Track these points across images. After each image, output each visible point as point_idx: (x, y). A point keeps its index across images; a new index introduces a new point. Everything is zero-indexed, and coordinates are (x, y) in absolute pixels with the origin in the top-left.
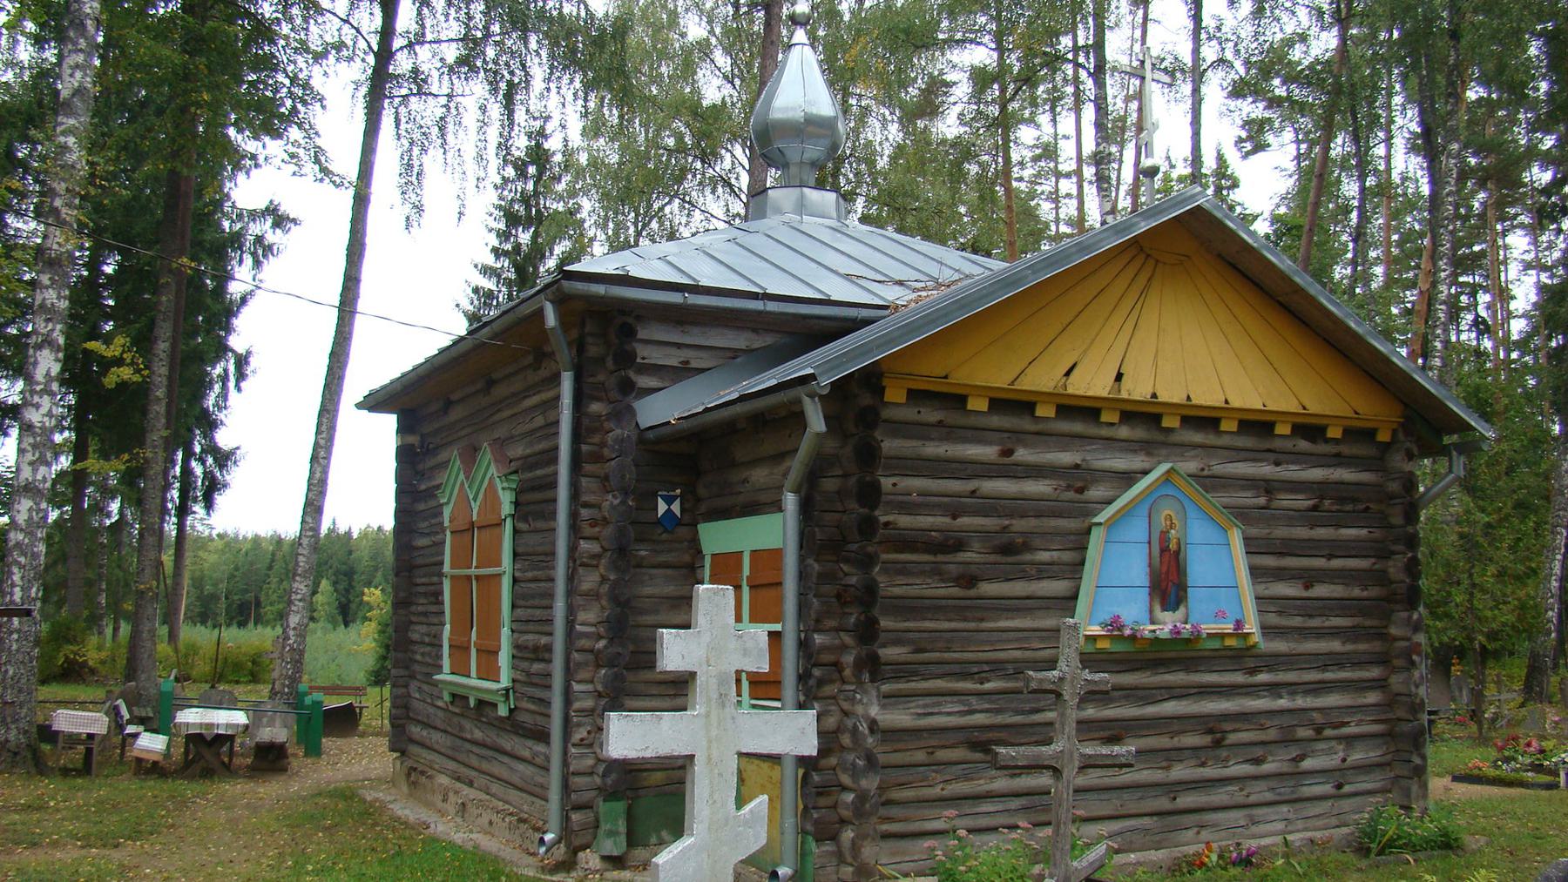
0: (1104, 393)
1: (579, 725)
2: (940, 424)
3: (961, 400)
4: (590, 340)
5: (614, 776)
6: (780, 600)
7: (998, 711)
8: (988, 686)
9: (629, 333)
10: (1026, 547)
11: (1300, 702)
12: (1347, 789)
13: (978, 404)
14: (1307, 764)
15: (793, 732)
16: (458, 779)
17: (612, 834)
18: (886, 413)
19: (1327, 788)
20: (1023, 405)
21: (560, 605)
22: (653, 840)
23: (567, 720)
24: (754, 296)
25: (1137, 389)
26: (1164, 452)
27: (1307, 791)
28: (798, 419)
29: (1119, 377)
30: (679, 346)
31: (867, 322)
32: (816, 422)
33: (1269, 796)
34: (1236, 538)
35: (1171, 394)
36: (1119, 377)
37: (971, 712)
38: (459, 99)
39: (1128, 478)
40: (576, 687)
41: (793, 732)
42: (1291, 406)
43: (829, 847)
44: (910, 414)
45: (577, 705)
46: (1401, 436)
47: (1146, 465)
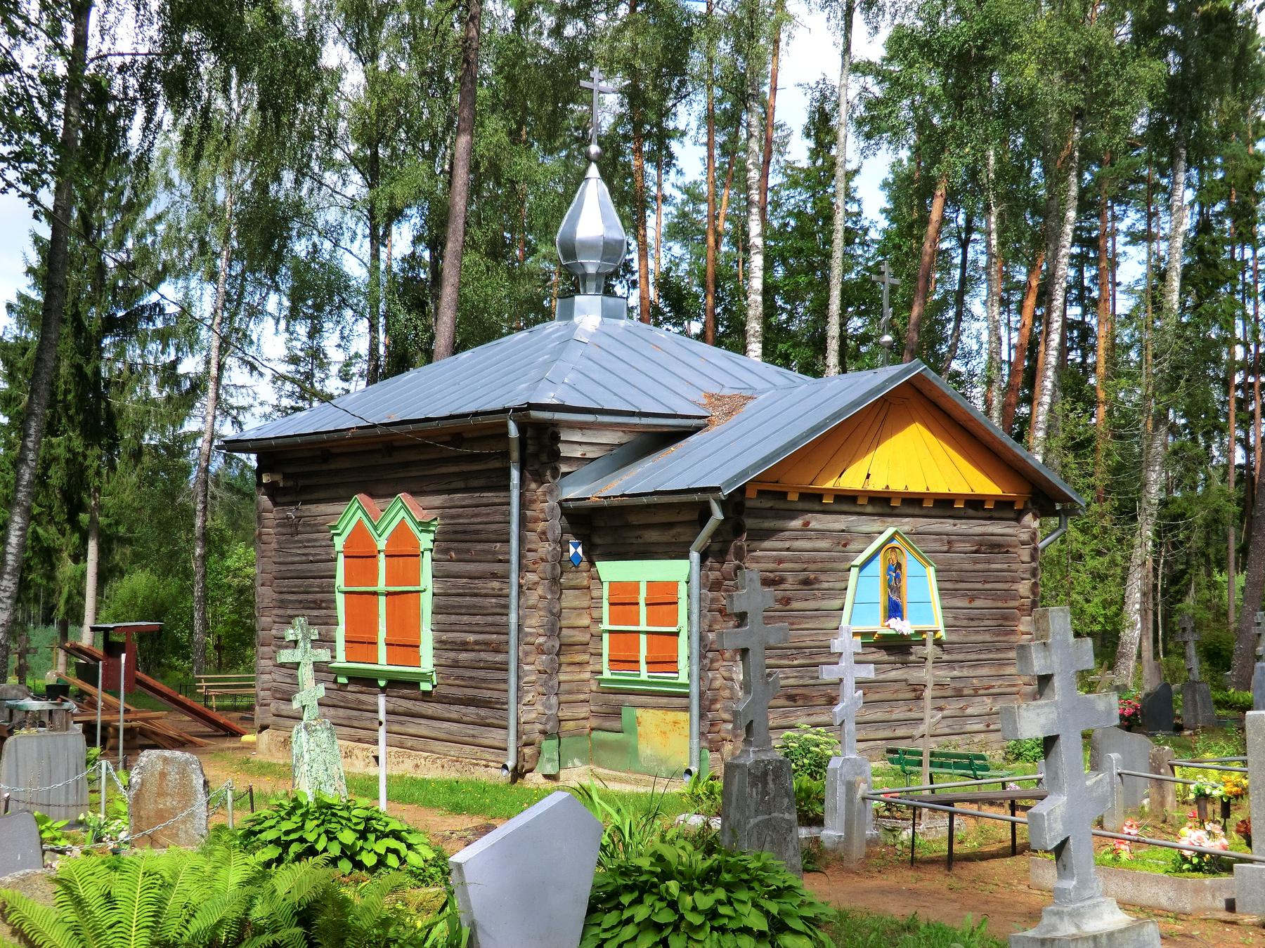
0: (859, 488)
1: (528, 692)
2: (771, 508)
3: (783, 495)
4: (529, 442)
5: (551, 723)
6: (675, 614)
7: (802, 677)
8: (796, 662)
9: (556, 438)
10: (817, 580)
11: (965, 673)
12: (992, 727)
13: (793, 497)
14: (969, 711)
15: (828, 674)
16: (359, 740)
17: (550, 760)
18: (748, 504)
19: (981, 727)
20: (817, 496)
21: (513, 618)
22: (570, 765)
23: (518, 688)
24: (632, 414)
25: (877, 485)
26: (890, 520)
27: (969, 728)
28: (706, 514)
29: (868, 476)
30: (580, 443)
31: (698, 429)
32: (718, 514)
33: (947, 731)
34: (931, 571)
35: (898, 486)
36: (868, 476)
37: (787, 678)
38: (23, 42)
39: (870, 537)
40: (526, 668)
41: (828, 674)
42: (965, 490)
43: (717, 755)
44: (757, 504)
45: (526, 679)
46: (1030, 505)
47: (881, 529)
